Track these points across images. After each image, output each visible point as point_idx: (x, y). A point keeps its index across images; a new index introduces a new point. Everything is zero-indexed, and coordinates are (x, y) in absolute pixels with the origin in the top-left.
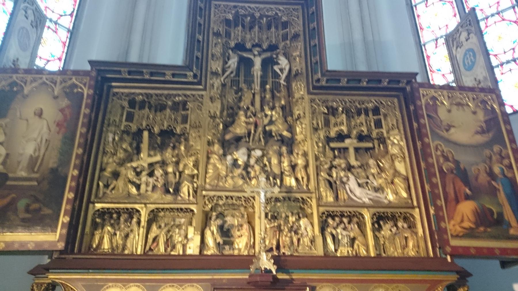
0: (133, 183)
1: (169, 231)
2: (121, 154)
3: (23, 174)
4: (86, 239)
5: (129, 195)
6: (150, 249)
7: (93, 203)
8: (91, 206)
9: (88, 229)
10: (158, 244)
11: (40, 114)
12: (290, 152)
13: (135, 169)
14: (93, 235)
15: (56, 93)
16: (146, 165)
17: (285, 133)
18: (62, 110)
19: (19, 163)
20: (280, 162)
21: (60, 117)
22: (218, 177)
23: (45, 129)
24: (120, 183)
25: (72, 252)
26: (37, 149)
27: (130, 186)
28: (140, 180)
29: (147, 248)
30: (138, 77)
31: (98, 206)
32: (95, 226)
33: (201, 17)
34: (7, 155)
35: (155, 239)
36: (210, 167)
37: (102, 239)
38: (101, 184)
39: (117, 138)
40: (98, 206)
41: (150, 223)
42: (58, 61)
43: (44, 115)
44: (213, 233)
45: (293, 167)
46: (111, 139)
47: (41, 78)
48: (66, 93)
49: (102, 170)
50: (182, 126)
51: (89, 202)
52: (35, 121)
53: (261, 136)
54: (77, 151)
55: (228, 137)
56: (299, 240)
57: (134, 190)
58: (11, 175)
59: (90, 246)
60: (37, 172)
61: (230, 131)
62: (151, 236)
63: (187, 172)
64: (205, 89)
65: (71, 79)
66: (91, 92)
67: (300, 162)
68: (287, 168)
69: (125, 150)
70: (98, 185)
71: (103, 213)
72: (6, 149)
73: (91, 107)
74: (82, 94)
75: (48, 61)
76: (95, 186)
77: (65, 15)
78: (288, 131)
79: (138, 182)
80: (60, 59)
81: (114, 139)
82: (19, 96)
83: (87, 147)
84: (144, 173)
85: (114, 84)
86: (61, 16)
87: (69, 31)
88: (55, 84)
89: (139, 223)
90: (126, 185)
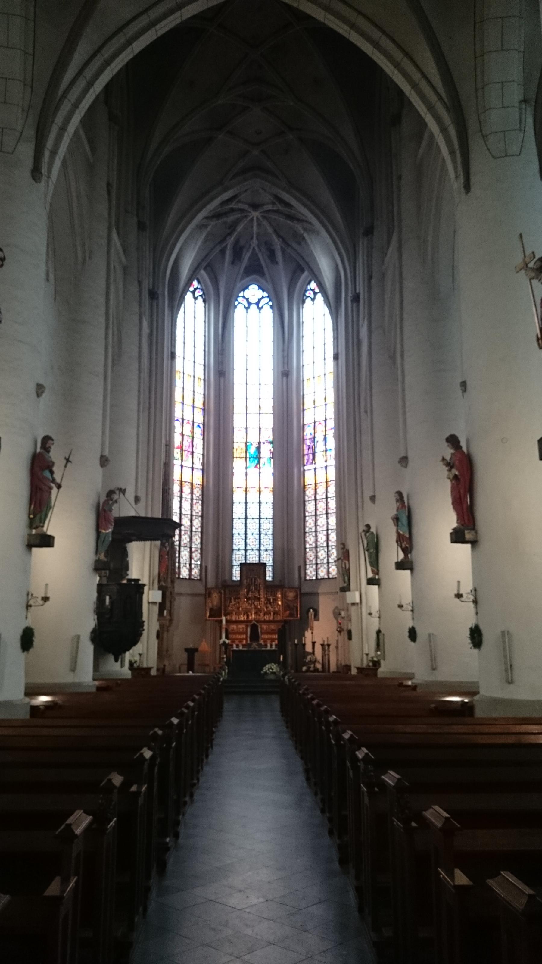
45: (260, 604)
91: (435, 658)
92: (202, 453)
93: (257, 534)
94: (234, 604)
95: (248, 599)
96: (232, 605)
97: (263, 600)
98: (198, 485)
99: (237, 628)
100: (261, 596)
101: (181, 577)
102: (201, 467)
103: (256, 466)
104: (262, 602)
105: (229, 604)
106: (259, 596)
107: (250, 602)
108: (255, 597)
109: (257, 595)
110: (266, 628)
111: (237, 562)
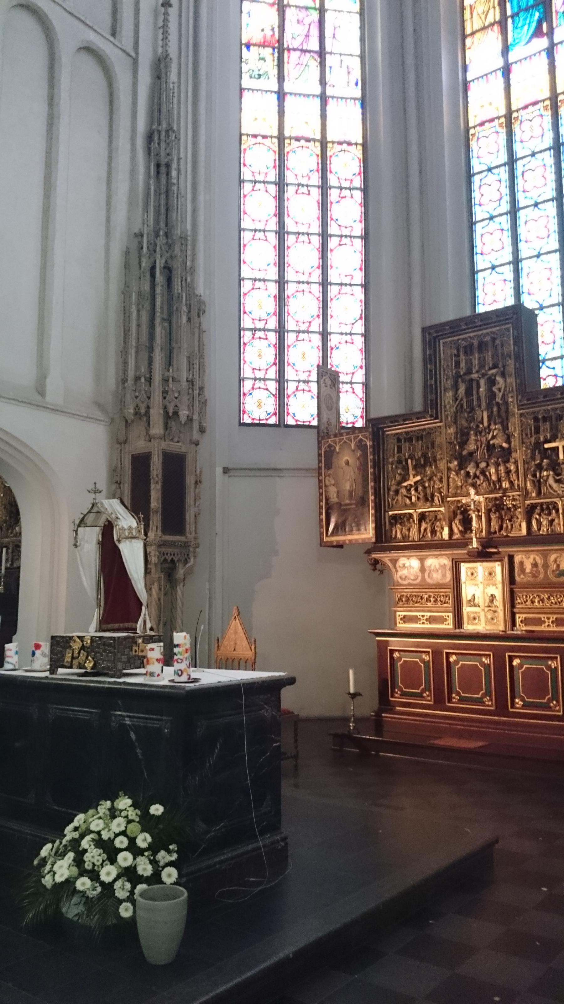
0: (407, 497)
1: (433, 524)
2: (398, 478)
3: (348, 502)
4: (389, 534)
5: (406, 505)
6: (423, 536)
7: (388, 512)
8: (387, 514)
9: (387, 528)
10: (427, 533)
11: (347, 463)
12: (507, 461)
13: (406, 487)
14: (391, 531)
15: (353, 448)
16: (413, 483)
17: (505, 445)
18: (358, 459)
19: (344, 496)
20: (497, 471)
21: (358, 463)
22: (457, 488)
23: (352, 473)
24: (400, 498)
25: (382, 542)
26: (351, 486)
27: (406, 498)
28: (411, 494)
29: (421, 536)
30: (396, 424)
31: (390, 513)
32: (391, 525)
33: (431, 363)
34: (338, 492)
35: (425, 530)
36: (451, 480)
37: (396, 532)
38: (390, 500)
39: (394, 466)
40: (390, 513)
41: (420, 521)
42: (360, 369)
43: (350, 463)
44: (456, 525)
45: (508, 472)
46: (390, 469)
47: (343, 439)
48: (358, 446)
49: (389, 490)
50: (431, 451)
51: (385, 511)
52: (346, 468)
53: (485, 451)
54: (371, 484)
55: (465, 453)
56: (512, 525)
57: (408, 501)
58: (343, 503)
59: (391, 536)
60: (354, 500)
61: (465, 449)
62: (422, 529)
63: (436, 486)
64: (441, 421)
65: (358, 436)
66: (371, 443)
67: (512, 467)
68: (503, 475)
69: (400, 474)
70: (388, 501)
71: (395, 517)
72: (337, 488)
73: (373, 454)
74: (366, 445)
75: (353, 373)
76: (386, 501)
77: (357, 321)
78: (506, 442)
79: (409, 495)
80: (361, 367)
81: (392, 468)
82: (335, 453)
83: (377, 479)
84: (412, 489)
85: (385, 429)
86: (353, 324)
87: (362, 335)
88: (351, 441)
89: (414, 521)
90: (402, 498)
91: (281, 476)
92: (358, 52)
93: (555, 251)
94: (416, 483)
95: (463, 461)
96: (408, 489)
97: (519, 455)
98: (345, 145)
99: (423, 569)
100: (515, 443)
101: (290, 421)
102: (357, 93)
103: (538, 33)
104: (516, 463)
105: (399, 483)
106: (505, 445)
107: (471, 469)
108: (490, 448)
109: (500, 441)
110: (535, 565)
111: (552, 372)
